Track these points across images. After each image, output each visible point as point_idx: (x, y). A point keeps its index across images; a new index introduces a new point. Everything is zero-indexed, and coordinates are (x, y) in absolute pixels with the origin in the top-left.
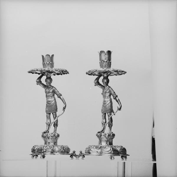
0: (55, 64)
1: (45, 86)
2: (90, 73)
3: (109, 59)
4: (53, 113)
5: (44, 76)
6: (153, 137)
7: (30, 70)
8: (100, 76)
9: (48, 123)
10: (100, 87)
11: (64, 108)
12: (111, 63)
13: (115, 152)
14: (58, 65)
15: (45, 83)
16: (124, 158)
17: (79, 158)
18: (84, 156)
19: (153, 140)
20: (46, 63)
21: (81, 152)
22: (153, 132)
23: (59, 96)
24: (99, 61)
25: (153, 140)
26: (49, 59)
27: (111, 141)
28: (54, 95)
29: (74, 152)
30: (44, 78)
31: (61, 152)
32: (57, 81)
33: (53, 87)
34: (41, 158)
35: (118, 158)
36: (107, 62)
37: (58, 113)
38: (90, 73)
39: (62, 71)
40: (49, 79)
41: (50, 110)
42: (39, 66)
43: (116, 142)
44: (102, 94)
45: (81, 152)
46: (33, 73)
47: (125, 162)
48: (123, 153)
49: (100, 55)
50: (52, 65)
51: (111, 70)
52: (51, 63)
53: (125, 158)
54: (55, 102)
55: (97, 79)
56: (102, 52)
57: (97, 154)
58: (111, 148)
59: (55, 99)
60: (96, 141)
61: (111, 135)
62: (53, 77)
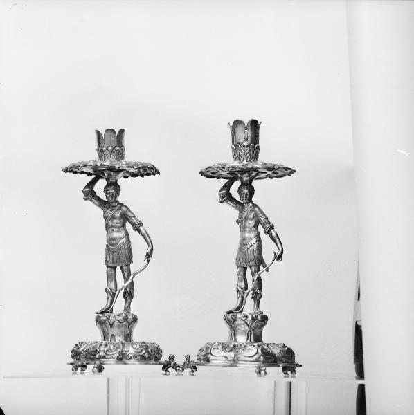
0: (126, 153)
1: (102, 203)
3: (255, 139)
4: (121, 268)
6: (359, 324)
7: (67, 165)
8: (232, 178)
10: (97, 203)
11: (149, 255)
13: (269, 359)
14: (134, 154)
15: (103, 197)
16: (289, 372)
19: (358, 331)
20: (107, 149)
22: (357, 311)
23: (137, 226)
24: (230, 145)
25: (358, 331)
27: (258, 331)
28: (124, 225)
29: (172, 358)
30: (102, 183)
32: (131, 191)
33: (122, 205)
36: (248, 146)
38: (209, 173)
39: (144, 168)
40: (113, 186)
43: (270, 335)
48: (286, 360)
50: (120, 154)
53: (292, 372)
56: (237, 123)
60: (223, 333)
61: (259, 317)
62: (121, 181)
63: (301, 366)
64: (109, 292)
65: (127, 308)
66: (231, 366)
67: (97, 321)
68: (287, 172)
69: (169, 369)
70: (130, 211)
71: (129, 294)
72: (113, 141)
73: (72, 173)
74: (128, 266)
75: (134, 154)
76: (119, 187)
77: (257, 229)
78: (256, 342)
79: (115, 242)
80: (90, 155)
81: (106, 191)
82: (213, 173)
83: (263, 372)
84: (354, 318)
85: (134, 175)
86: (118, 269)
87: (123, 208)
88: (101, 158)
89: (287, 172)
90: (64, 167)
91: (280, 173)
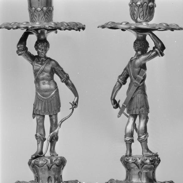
0: (55, 13)
1: (33, 58)
4: (50, 116)
5: (30, 36)
9: (41, 135)
10: (30, 59)
11: (75, 105)
15: (35, 53)
20: (42, 10)
23: (66, 80)
28: (52, 78)
30: (32, 39)
31: (127, 74)
33: (51, 60)
36: (142, 5)
37: (60, 116)
40: (42, 42)
44: (130, 5)
46: (9, 29)
50: (48, 13)
51: (154, 21)
52: (45, 8)
55: (23, 40)
59: (56, 87)
61: (148, 161)
62: (50, 37)
63: (70, 103)
64: (40, 137)
65: (52, 151)
67: (30, 164)
70: (116, 85)
71: (54, 139)
74: (56, 115)
79: (47, 93)
86: (47, 117)
87: (53, 62)
88: (32, 20)
91: (133, 17)
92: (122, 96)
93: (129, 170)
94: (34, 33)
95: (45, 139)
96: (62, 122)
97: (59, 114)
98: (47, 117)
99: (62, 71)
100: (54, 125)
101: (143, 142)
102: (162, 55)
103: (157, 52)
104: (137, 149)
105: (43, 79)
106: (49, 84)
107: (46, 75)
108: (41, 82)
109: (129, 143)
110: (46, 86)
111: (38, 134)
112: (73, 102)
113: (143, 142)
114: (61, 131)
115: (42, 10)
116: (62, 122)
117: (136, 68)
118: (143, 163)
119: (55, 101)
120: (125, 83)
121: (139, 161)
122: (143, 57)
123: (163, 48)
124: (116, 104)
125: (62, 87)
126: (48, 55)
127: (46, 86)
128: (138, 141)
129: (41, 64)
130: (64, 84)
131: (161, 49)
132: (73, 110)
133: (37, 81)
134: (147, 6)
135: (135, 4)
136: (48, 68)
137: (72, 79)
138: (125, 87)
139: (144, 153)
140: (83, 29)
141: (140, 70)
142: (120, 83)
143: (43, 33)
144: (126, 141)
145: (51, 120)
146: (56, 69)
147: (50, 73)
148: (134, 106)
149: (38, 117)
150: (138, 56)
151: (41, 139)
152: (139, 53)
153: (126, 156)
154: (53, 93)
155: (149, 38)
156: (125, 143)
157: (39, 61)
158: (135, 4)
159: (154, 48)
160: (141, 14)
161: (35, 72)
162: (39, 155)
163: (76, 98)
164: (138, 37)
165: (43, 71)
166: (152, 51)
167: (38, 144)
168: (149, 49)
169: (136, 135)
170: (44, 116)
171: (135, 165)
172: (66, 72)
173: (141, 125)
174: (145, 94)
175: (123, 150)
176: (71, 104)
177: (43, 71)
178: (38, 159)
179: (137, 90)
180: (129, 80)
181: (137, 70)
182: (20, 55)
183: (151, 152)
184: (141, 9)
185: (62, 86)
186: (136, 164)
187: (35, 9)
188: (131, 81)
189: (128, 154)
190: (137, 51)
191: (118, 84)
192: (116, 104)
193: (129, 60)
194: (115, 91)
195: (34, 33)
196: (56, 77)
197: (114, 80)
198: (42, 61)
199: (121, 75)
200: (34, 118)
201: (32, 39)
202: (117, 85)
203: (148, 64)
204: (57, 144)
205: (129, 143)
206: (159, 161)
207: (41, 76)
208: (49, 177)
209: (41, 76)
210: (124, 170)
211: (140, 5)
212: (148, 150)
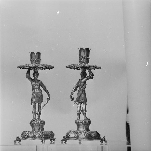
1: (32, 80)
2: (23, 67)
3: (88, 55)
4: (38, 104)
6: (128, 122)
7: (19, 66)
8: (30, 69)
12: (89, 59)
13: (90, 138)
14: (44, 61)
15: (33, 78)
16: (53, 141)
17: (45, 143)
18: (21, 141)
19: (128, 126)
21: (18, 137)
22: (127, 118)
24: (78, 56)
25: (128, 126)
26: (35, 57)
27: (87, 126)
29: (104, 138)
30: (32, 72)
32: (43, 75)
34: (54, 144)
35: (47, 141)
36: (85, 57)
37: (43, 104)
38: (70, 67)
39: (96, 67)
40: (36, 73)
41: (38, 100)
42: (27, 62)
43: (92, 128)
45: (18, 137)
47: (103, 146)
48: (97, 137)
49: (80, 53)
50: (39, 61)
53: (54, 141)
54: (42, 94)
55: (28, 72)
56: (81, 49)
57: (74, 138)
58: (85, 134)
59: (42, 92)
60: (75, 127)
61: (87, 122)
62: (39, 71)
66: (76, 140)
68: (51, 67)
69: (103, 142)
72: (35, 57)
73: (43, 70)
75: (44, 61)
76: (38, 74)
77: (40, 88)
78: (87, 131)
80: (27, 62)
81: (34, 74)
82: (72, 67)
83: (44, 142)
84: (126, 120)
85: (45, 69)
86: (37, 104)
87: (40, 82)
89: (51, 67)
90: (67, 65)
92: (75, 96)
93: (78, 125)
94: (33, 69)
95: (36, 113)
96: (43, 106)
97: (42, 103)
98: (37, 104)
99: (44, 85)
100: (40, 108)
101: (85, 114)
102: (93, 78)
103: (91, 77)
104: (82, 117)
105: (36, 88)
106: (39, 90)
107: (37, 87)
108: (35, 90)
109: (79, 115)
110: (37, 91)
111: (34, 111)
112: (48, 98)
113: (85, 114)
114: (42, 111)
115: (37, 60)
116: (43, 106)
117: (82, 83)
118: (85, 122)
119: (41, 97)
120: (76, 90)
121: (83, 122)
122: (85, 79)
123: (93, 75)
124: (72, 99)
125: (44, 92)
126: (38, 79)
127: (37, 91)
128: (82, 114)
129: (35, 82)
130: (44, 91)
131: (92, 76)
132: (48, 101)
133: (33, 89)
134: (87, 58)
135: (82, 57)
136: (38, 84)
137: (48, 89)
138: (77, 92)
139: (85, 119)
140: (54, 67)
141: (84, 84)
142: (75, 90)
143: (37, 69)
144: (77, 114)
145: (39, 105)
146: (41, 85)
147: (39, 86)
148: (81, 99)
149: (34, 104)
150: (82, 79)
151: (34, 113)
152: (83, 77)
153: (78, 120)
154: (41, 94)
155: (87, 71)
156: (77, 114)
157: (34, 81)
158: (82, 57)
159: (89, 75)
160: (84, 61)
161: (33, 86)
162: (34, 120)
163: (49, 96)
164: (82, 71)
165: (36, 85)
166: (89, 76)
167: (33, 115)
168: (87, 76)
169: (81, 112)
170: (36, 104)
171: (82, 123)
172: (45, 86)
173: (83, 107)
174: (85, 94)
175: (76, 117)
176: (47, 99)
177: (36, 85)
178: (34, 121)
179: (82, 92)
180: (78, 89)
181: (82, 84)
182: (27, 78)
183: (87, 118)
184: (84, 59)
185: (44, 92)
186: (82, 123)
187: (34, 59)
188: (80, 89)
189: (79, 119)
190: (82, 77)
191: (74, 90)
192: (72, 99)
193: (79, 80)
194: (72, 93)
195: (33, 69)
196: (41, 88)
197: (72, 89)
198: (36, 81)
199: (75, 87)
200: (31, 105)
201: (32, 72)
202: (73, 91)
203: (87, 82)
204: (41, 115)
205: (79, 115)
206: (91, 122)
207: (35, 87)
208: (39, 129)
209: (35, 87)
210: (76, 126)
211: (84, 58)
212: (87, 118)
